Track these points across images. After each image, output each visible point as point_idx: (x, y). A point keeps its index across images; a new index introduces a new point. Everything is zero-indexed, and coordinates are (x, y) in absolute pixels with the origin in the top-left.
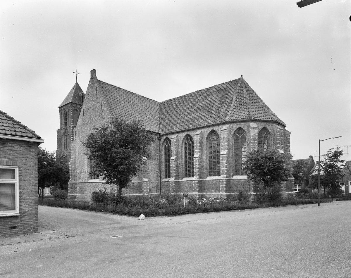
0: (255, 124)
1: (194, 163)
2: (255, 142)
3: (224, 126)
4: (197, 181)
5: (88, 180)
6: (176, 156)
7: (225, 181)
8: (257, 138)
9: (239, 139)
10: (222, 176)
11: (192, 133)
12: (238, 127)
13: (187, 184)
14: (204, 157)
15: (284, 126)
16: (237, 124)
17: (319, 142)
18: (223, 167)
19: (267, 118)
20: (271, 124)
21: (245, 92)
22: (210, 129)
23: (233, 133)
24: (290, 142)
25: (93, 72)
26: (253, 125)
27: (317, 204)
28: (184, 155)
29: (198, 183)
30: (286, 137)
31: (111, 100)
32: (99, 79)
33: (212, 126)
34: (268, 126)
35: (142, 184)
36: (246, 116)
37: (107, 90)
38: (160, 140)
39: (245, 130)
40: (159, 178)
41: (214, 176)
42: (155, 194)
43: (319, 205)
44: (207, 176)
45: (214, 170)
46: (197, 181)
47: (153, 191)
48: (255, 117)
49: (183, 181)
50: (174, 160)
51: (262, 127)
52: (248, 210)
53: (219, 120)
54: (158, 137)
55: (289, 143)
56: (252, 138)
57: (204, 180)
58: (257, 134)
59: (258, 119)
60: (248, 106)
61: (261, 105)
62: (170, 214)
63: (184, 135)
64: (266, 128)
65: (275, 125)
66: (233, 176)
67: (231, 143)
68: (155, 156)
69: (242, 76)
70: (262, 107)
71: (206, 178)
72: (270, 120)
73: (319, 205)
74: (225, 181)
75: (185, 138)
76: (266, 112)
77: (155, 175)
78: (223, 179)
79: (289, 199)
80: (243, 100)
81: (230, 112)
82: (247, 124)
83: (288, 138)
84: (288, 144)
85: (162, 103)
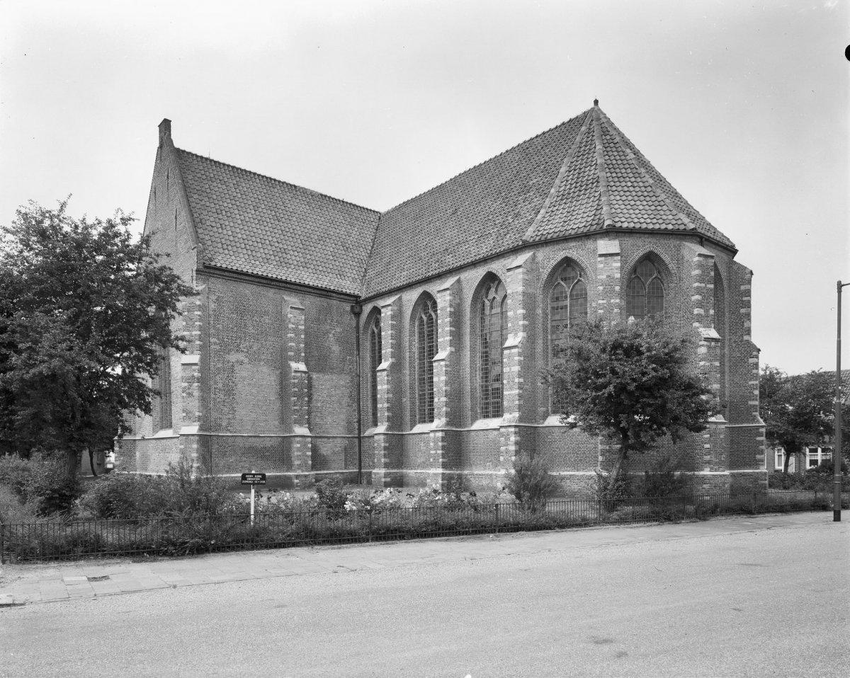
0: (616, 242)
1: (435, 379)
2: (612, 301)
3: (519, 257)
4: (440, 434)
5: (155, 431)
6: (394, 360)
7: (515, 433)
8: (617, 288)
9: (566, 297)
10: (507, 416)
11: (433, 288)
12: (561, 255)
13: (422, 444)
14: (467, 360)
15: (732, 251)
16: (557, 247)
17: (840, 292)
18: (511, 389)
19: (661, 221)
20: (673, 242)
21: (599, 147)
22: (480, 272)
23: (545, 276)
24: (749, 302)
25: (166, 126)
26: (607, 245)
27: (831, 515)
28: (416, 356)
29: (443, 439)
30: (729, 287)
31: (208, 204)
32: (176, 145)
33: (485, 260)
34: (663, 249)
35: (291, 443)
36: (589, 219)
37: (204, 177)
38: (358, 315)
39: (583, 265)
40: (356, 425)
41: (494, 416)
42: (342, 473)
43: (837, 518)
44: (474, 419)
45: (496, 400)
46: (440, 434)
47: (333, 465)
48: (617, 219)
49: (414, 434)
50: (386, 372)
51: (641, 253)
52: (514, 534)
53: (508, 242)
54: (352, 307)
55: (748, 305)
56: (601, 288)
57: (466, 429)
58: (618, 276)
59: (625, 225)
60: (600, 188)
61: (647, 184)
62: (149, 553)
63: (412, 296)
64: (657, 255)
65: (686, 243)
66: (545, 417)
67: (539, 311)
68: (344, 360)
69: (596, 102)
70: (649, 189)
71: (472, 424)
72: (670, 227)
73: (837, 518)
74: (515, 433)
75: (419, 305)
76: (662, 203)
77: (343, 416)
78: (510, 426)
79: (734, 491)
80: (591, 172)
81: (542, 211)
82: (590, 244)
83: (743, 288)
84: (743, 311)
85: (388, 212)
